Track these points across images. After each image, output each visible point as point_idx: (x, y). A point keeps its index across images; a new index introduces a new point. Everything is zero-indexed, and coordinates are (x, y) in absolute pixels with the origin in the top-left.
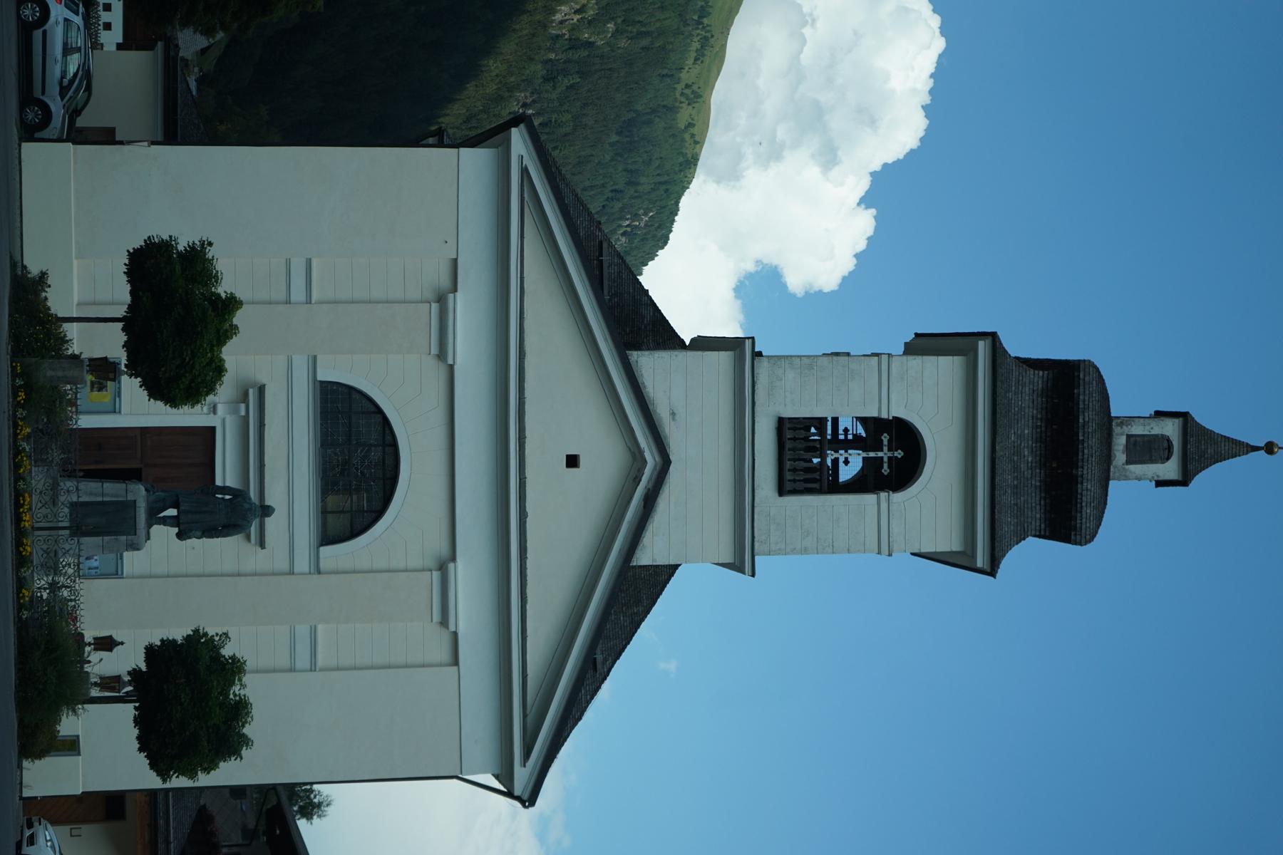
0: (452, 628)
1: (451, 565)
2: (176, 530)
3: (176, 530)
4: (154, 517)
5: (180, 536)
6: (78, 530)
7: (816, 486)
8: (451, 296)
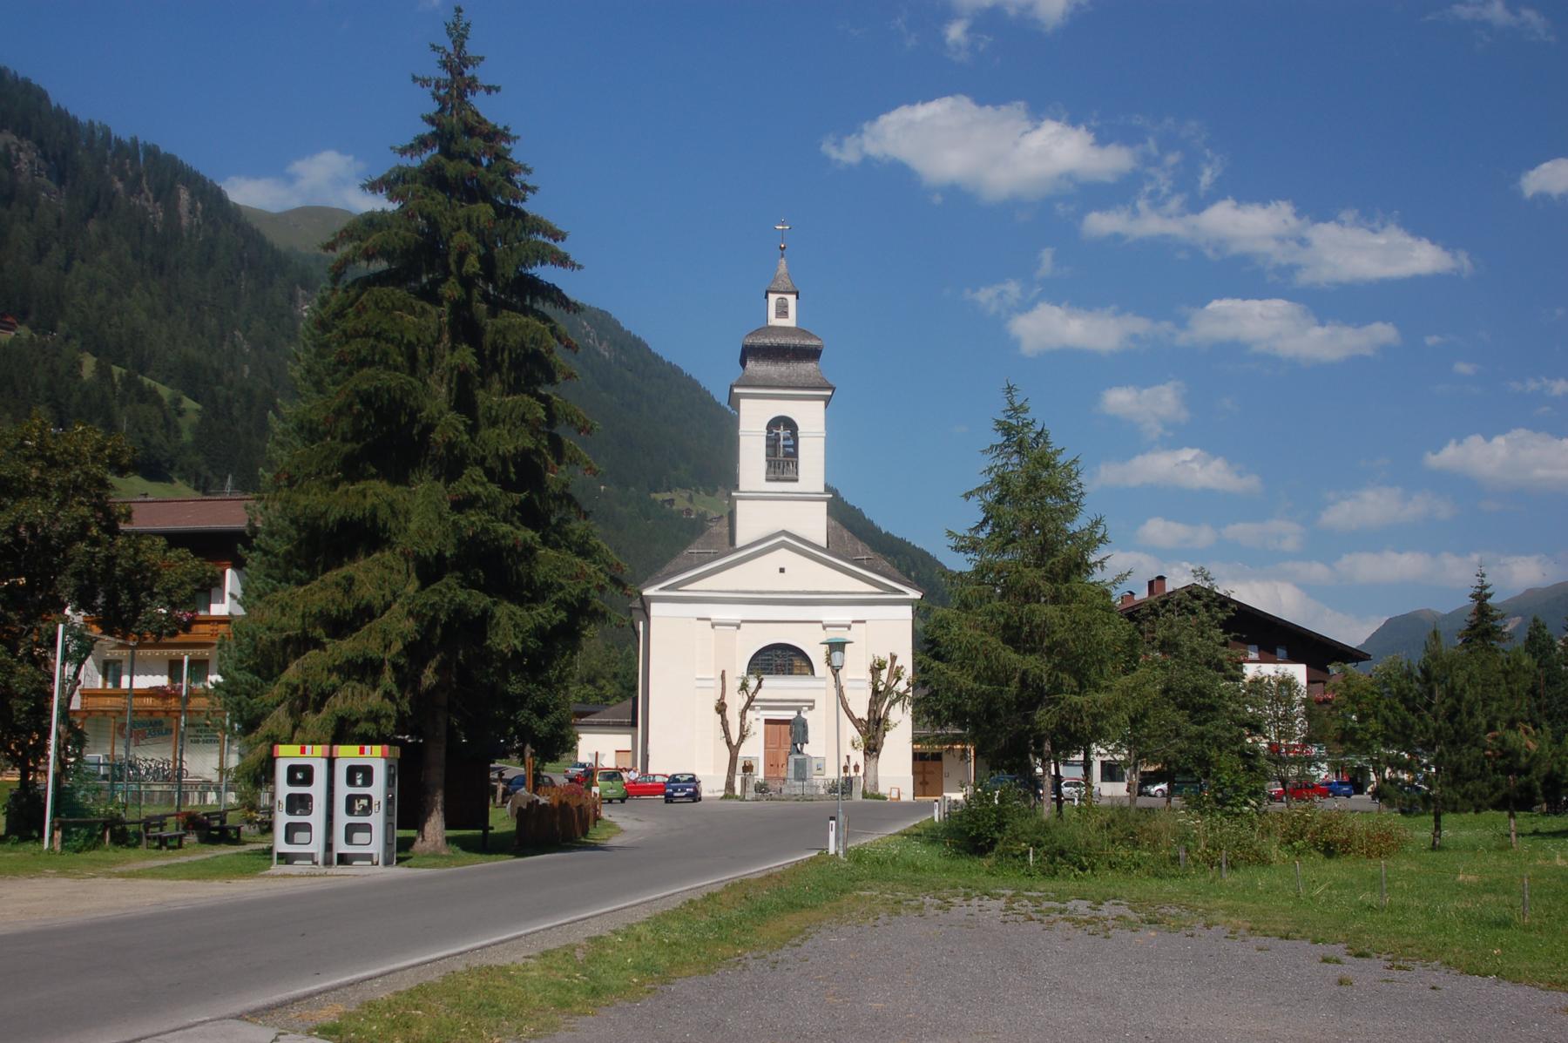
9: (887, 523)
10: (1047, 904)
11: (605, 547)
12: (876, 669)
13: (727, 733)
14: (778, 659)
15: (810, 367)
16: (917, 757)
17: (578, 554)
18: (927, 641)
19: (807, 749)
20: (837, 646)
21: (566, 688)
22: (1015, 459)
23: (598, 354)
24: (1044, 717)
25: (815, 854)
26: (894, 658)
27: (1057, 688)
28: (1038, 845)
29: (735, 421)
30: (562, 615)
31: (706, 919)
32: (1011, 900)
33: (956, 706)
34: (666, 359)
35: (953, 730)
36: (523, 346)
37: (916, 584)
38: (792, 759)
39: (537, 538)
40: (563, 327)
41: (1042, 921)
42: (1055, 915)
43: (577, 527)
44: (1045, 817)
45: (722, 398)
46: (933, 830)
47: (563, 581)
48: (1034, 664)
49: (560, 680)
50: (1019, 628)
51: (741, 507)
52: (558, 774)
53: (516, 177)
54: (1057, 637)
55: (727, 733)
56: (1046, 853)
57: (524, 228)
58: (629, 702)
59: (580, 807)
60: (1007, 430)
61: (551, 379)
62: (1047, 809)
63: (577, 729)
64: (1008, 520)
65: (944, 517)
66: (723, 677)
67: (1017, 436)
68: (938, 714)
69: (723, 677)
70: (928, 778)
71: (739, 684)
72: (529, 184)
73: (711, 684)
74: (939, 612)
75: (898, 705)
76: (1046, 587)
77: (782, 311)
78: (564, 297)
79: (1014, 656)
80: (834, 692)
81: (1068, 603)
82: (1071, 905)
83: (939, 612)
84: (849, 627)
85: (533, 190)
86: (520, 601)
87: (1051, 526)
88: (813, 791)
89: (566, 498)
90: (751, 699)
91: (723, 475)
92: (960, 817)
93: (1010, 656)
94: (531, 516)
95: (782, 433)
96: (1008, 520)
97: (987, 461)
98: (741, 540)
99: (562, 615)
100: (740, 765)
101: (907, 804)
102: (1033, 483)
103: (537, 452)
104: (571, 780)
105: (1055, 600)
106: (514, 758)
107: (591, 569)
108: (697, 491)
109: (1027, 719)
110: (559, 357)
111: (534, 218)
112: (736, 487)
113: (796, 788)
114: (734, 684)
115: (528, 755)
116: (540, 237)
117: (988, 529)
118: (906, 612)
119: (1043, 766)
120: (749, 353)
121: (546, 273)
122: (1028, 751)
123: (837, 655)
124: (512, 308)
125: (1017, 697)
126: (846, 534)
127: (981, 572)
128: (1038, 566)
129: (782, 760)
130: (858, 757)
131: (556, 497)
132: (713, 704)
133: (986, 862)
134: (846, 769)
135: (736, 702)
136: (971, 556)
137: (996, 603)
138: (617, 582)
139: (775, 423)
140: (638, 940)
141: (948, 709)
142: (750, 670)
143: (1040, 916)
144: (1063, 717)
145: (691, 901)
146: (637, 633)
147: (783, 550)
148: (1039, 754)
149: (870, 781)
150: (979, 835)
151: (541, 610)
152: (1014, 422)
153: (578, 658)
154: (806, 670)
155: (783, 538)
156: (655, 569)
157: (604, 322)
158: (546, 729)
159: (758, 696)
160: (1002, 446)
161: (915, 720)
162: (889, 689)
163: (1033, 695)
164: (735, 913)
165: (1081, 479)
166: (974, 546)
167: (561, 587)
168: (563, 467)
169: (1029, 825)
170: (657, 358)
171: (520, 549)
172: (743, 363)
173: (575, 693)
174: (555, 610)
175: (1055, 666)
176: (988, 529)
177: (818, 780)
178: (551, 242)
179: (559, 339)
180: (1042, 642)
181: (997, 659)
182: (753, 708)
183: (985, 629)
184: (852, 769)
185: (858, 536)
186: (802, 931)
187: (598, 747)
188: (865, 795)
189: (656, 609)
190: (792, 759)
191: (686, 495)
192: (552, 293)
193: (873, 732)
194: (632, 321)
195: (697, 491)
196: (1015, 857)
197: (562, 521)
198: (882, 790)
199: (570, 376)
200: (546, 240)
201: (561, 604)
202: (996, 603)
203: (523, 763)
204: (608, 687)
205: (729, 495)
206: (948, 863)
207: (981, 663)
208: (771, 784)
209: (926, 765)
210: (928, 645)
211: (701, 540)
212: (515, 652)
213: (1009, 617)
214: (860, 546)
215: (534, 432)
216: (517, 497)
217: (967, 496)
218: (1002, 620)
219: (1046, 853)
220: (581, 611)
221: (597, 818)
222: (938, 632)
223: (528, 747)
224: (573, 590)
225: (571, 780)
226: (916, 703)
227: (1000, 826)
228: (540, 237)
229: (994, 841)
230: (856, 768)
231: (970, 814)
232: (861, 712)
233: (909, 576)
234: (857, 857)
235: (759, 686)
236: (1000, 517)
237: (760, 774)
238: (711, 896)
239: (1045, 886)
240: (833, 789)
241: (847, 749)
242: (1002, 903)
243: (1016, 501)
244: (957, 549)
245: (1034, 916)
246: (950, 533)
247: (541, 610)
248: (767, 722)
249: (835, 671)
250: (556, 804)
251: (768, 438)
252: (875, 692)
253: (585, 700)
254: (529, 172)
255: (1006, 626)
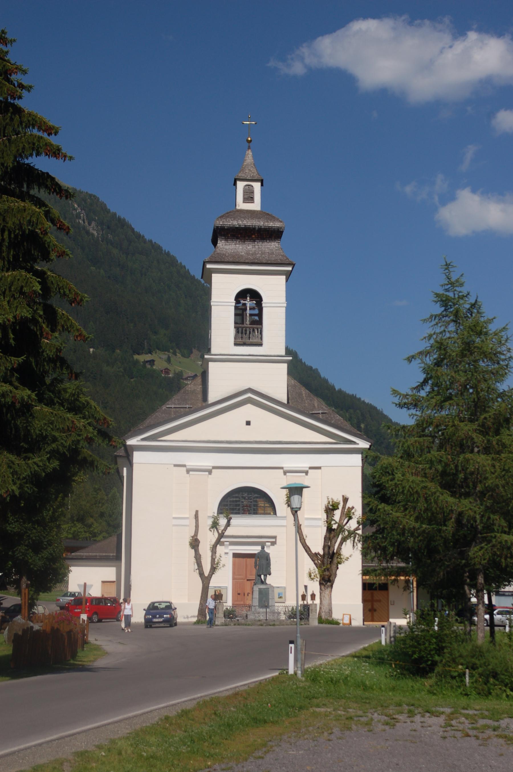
0: (307, 469)
1: (285, 469)
2: (268, 575)
3: (268, 575)
4: (263, 582)
5: (270, 574)
6: (267, 607)
7: (259, 330)
8: (187, 467)
9: (342, 379)
10: (482, 722)
11: (93, 403)
12: (330, 509)
13: (198, 558)
14: (246, 501)
15: (272, 246)
16: (367, 587)
17: (70, 410)
18: (375, 485)
19: (269, 580)
20: (295, 491)
21: (59, 527)
22: (452, 327)
23: (88, 233)
24: (478, 553)
25: (276, 674)
26: (345, 500)
27: (489, 528)
28: (473, 667)
29: (207, 292)
30: (55, 464)
31: (179, 734)
32: (450, 717)
33: (400, 543)
34: (147, 237)
35: (397, 564)
36: (21, 225)
37: (365, 435)
38: (256, 589)
39: (33, 396)
40: (56, 212)
41: (477, 738)
42: (489, 732)
43: (70, 386)
44: (480, 642)
45: (197, 274)
46: (380, 652)
47: (57, 434)
48: (469, 507)
49: (54, 519)
50: (455, 475)
51: (212, 367)
52: (45, 607)
53: (13, 77)
54: (489, 483)
55: (198, 558)
56: (481, 675)
57: (21, 123)
58: (114, 539)
59: (69, 632)
60: (445, 302)
61: (46, 257)
62: (481, 635)
63: (68, 562)
64: (446, 380)
65: (390, 379)
66: (196, 516)
67: (453, 307)
68: (384, 549)
69: (196, 516)
70: (376, 605)
71: (210, 522)
72: (25, 84)
73: (186, 522)
74: (386, 460)
75: (349, 542)
76: (479, 439)
77: (249, 198)
78: (57, 184)
79: (451, 500)
80: (293, 529)
81: (499, 453)
82: (503, 723)
83: (386, 460)
84: (307, 473)
85: (29, 88)
86: (17, 451)
87: (483, 385)
88: (275, 618)
89: (59, 361)
90: (221, 535)
91: (195, 339)
92: (404, 641)
93: (447, 499)
94: (28, 376)
95: (249, 303)
96: (446, 380)
97: (428, 329)
98: (212, 397)
99: (55, 464)
100: (211, 593)
101: (357, 630)
102: (468, 348)
103: (34, 320)
104: (62, 608)
105: (487, 450)
106: (12, 589)
107: (81, 423)
108: (175, 354)
109: (463, 555)
110: (53, 238)
111: (30, 114)
112: (209, 351)
113: (261, 614)
114: (206, 522)
115: (24, 586)
116: (35, 132)
117: (428, 388)
118: (357, 460)
119: (477, 596)
120: (220, 233)
121: (41, 163)
122: (464, 583)
123: (295, 499)
124: (12, 194)
125: (454, 535)
126: (304, 392)
127: (421, 426)
128: (471, 421)
129: (248, 590)
130: (315, 587)
131: (51, 360)
132: (187, 540)
133: (428, 682)
134: (304, 597)
135: (208, 538)
136: (413, 411)
137: (435, 453)
138: (104, 435)
139: (242, 295)
140: (120, 754)
141: (393, 545)
142: (221, 511)
143: (475, 732)
144: (494, 554)
145: (167, 718)
146: (121, 478)
147: (249, 406)
148: (473, 586)
149: (325, 608)
150: (421, 658)
151: (36, 460)
152: (451, 294)
153: (70, 500)
154: (269, 510)
155: (249, 395)
156: (137, 422)
157: (93, 206)
158: (40, 563)
159: (227, 533)
160: (440, 316)
161: (365, 554)
162: (341, 528)
163: (467, 534)
164: (206, 728)
165: (509, 345)
166: (415, 404)
167: (55, 439)
168: (57, 334)
169: (465, 649)
170: (139, 236)
171: (18, 406)
172: (215, 242)
173: (66, 530)
174: (49, 459)
175: (487, 508)
176: (428, 388)
177: (279, 607)
178: (45, 135)
179: (52, 221)
180: (475, 487)
181: (436, 502)
182: (222, 544)
183: (425, 476)
184: (309, 598)
185: (314, 392)
186: (265, 745)
187: (86, 579)
188: (321, 621)
189: (137, 457)
190: (256, 589)
191: (165, 357)
192: (46, 180)
193: (327, 565)
194: (117, 206)
195: (175, 354)
196: (453, 678)
197: (57, 381)
198: (336, 615)
199: (62, 254)
200: (40, 134)
201: (54, 454)
202: (435, 453)
203: (19, 593)
204: (95, 525)
205: (202, 357)
206: (393, 683)
207: (422, 505)
208: (238, 611)
209: (374, 594)
210: (375, 489)
211: (176, 397)
212: (13, 496)
213: (447, 465)
214: (316, 402)
215: (31, 300)
216: (16, 361)
217: (410, 359)
218: (440, 468)
219: (481, 675)
220: (72, 461)
221: (85, 642)
222: (384, 479)
223: (24, 579)
224: (66, 441)
225: (62, 608)
226: (365, 539)
227: (440, 650)
228: (35, 132)
229: (434, 664)
230: (313, 596)
231: (412, 639)
232: (318, 547)
233: (359, 428)
234: (314, 677)
235: (228, 525)
236: (438, 378)
237: (228, 602)
238: (185, 713)
239: (479, 705)
240: (292, 615)
241: (305, 580)
242: (441, 720)
243: (453, 364)
244: (401, 406)
245: (471, 732)
246: (395, 392)
247: (36, 460)
248: (236, 556)
249: (295, 512)
250: (48, 629)
251: (236, 308)
252: (330, 530)
253: (75, 537)
254: (24, 72)
255: (444, 474)
